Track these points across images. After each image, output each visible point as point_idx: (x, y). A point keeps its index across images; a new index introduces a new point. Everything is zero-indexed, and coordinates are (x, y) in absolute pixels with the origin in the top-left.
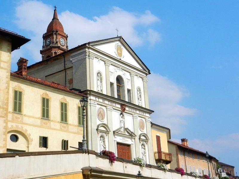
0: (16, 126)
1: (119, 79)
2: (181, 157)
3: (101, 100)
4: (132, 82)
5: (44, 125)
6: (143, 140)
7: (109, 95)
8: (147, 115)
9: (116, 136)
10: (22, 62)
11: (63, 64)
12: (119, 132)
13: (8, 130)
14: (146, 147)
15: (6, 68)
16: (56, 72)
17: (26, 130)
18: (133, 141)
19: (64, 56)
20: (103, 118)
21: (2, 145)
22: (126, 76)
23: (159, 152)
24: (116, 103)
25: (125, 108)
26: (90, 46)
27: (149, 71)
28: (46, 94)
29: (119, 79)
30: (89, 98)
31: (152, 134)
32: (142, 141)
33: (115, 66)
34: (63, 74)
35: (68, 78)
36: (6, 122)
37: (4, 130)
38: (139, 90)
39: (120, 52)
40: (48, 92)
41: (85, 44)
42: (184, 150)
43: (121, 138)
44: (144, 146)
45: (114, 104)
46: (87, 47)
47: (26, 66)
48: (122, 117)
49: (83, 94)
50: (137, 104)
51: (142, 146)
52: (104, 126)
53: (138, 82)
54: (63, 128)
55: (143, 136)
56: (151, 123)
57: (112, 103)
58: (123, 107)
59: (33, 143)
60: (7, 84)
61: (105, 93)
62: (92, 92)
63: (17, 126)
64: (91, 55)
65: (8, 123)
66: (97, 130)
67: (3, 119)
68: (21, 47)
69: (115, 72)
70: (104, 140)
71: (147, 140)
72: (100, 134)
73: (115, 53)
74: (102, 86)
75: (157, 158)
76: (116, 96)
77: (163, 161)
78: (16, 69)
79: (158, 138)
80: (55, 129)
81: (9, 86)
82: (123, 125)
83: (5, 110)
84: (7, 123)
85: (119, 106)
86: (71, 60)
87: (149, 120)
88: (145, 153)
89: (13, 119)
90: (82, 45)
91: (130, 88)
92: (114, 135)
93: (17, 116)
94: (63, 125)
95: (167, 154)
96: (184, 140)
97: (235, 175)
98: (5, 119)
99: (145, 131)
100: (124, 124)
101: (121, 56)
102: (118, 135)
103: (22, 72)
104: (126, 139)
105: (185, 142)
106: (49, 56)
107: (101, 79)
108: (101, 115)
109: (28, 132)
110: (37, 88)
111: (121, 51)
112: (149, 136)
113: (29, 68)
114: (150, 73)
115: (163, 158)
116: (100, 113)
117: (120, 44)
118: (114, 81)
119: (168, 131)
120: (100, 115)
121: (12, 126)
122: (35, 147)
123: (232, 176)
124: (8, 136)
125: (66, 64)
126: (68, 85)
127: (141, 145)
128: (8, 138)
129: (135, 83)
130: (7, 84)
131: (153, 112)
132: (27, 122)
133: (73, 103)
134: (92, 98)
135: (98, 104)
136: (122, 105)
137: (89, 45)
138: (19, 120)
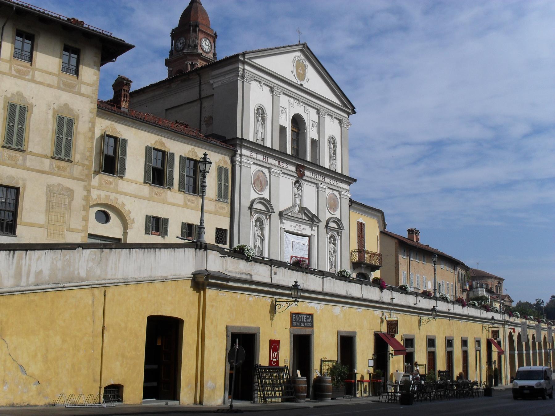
0: (106, 196)
1: (297, 121)
2: (403, 259)
3: (260, 157)
4: (320, 126)
5: (156, 197)
6: (333, 229)
7: (277, 147)
8: (345, 186)
9: (283, 221)
10: (121, 84)
11: (197, 89)
12: (290, 214)
13: (91, 204)
14: (338, 242)
15: (91, 95)
16: (185, 104)
17: (124, 205)
18: (314, 230)
19: (199, 75)
20: (262, 189)
21: (81, 228)
22: (310, 116)
23: (361, 250)
24: (288, 162)
25: (304, 173)
26: (246, 60)
27: (353, 108)
28: (160, 142)
29: (297, 121)
30: (239, 152)
31: (351, 220)
32: (331, 230)
33: (291, 97)
34: (196, 107)
35: (205, 115)
36: (88, 189)
37: (84, 203)
38: (332, 141)
39: (301, 72)
40: (164, 140)
41: (237, 56)
42: (410, 246)
43: (294, 224)
44: (335, 240)
45: (284, 165)
46: (241, 60)
47: (128, 91)
48: (298, 188)
49: (230, 143)
50: (327, 166)
51: (330, 239)
52: (266, 203)
53: (332, 128)
54: (189, 203)
55: (334, 222)
56: (351, 200)
57: (281, 163)
58: (301, 171)
59: (135, 225)
60: (90, 124)
61: (268, 144)
62: (245, 143)
63: (107, 197)
64: (246, 75)
65: (92, 190)
66: (250, 208)
67: (83, 183)
68: (118, 58)
69: (289, 107)
70: (262, 227)
71: (340, 227)
72: (256, 216)
73: (292, 72)
74: (264, 132)
75: (355, 258)
76: (289, 151)
77: (365, 266)
78: (110, 95)
79: (361, 226)
80: (174, 205)
81: (93, 126)
82: (298, 202)
83: (86, 169)
84: (89, 191)
85: (293, 168)
86: (211, 83)
87: (346, 194)
88: (335, 251)
89: (100, 184)
90: (231, 57)
91: (316, 138)
92: (281, 219)
93: (109, 180)
94: (189, 198)
95: (374, 254)
96: (413, 231)
97: (504, 293)
98: (86, 183)
99: (337, 215)
100: (300, 200)
101: (302, 80)
102: (288, 219)
103: (120, 102)
104: (303, 226)
105: (415, 235)
106: (180, 71)
107: (263, 120)
108: (259, 183)
109: (127, 208)
110: (145, 131)
111: (304, 71)
112: (345, 223)
113: (137, 92)
114: (354, 112)
115: (367, 260)
116: (258, 179)
117: (302, 57)
118: (287, 123)
119: (380, 215)
120: (258, 183)
121: (99, 196)
122: (137, 234)
123: (495, 294)
124: (90, 212)
125: (202, 89)
126: (204, 127)
127: (329, 237)
128: (90, 216)
129: (325, 129)
130: (90, 124)
131: (355, 180)
132: (123, 190)
133: (217, 159)
134: (245, 152)
135: (254, 163)
136: (298, 167)
137: (244, 57)
138: (112, 186)
